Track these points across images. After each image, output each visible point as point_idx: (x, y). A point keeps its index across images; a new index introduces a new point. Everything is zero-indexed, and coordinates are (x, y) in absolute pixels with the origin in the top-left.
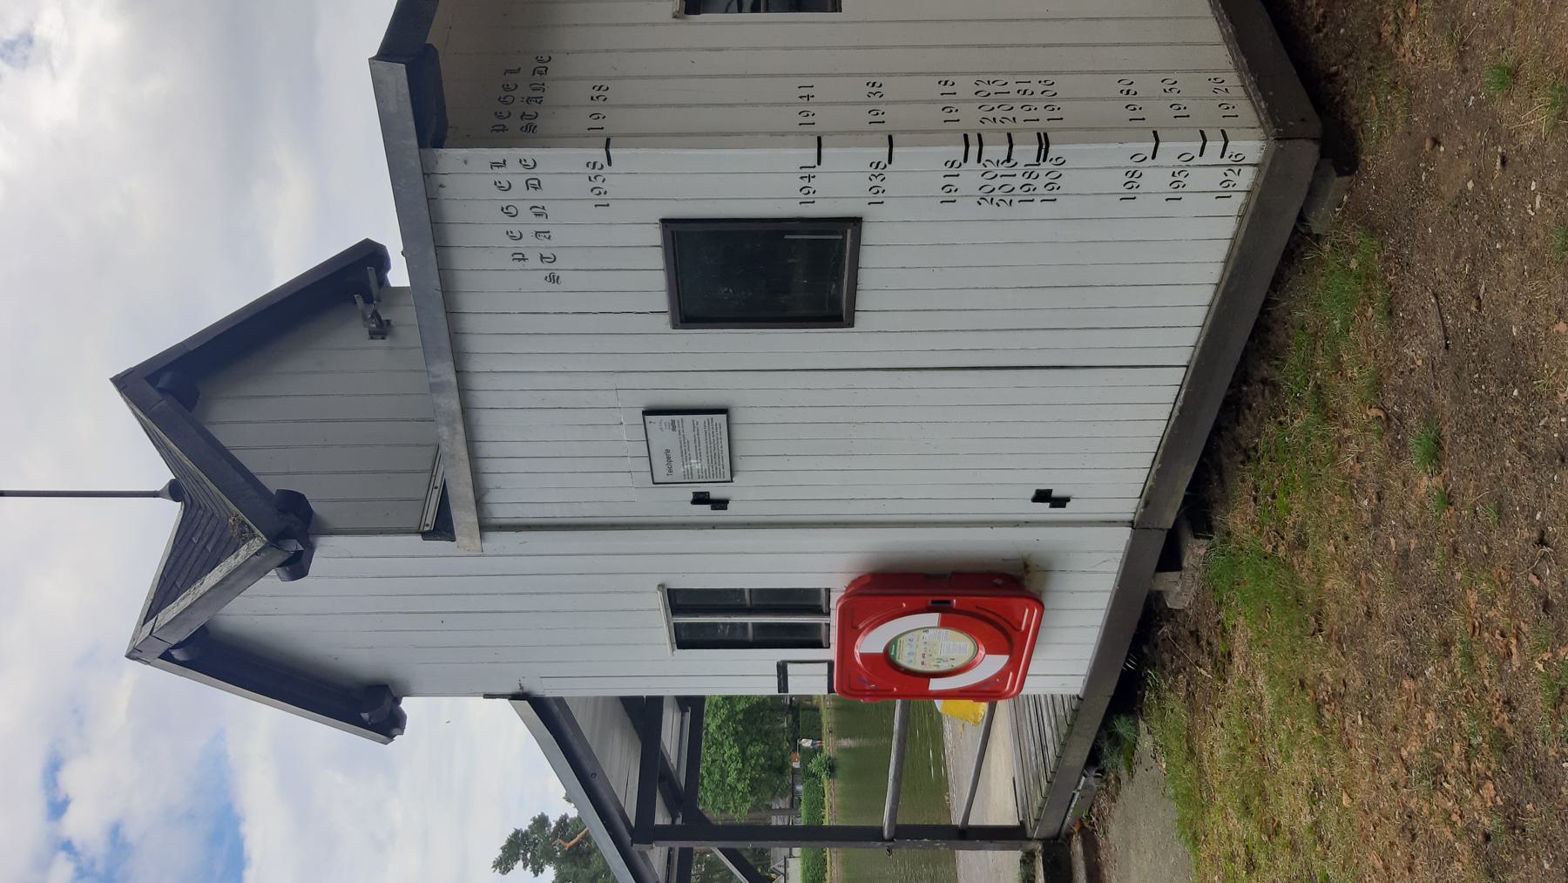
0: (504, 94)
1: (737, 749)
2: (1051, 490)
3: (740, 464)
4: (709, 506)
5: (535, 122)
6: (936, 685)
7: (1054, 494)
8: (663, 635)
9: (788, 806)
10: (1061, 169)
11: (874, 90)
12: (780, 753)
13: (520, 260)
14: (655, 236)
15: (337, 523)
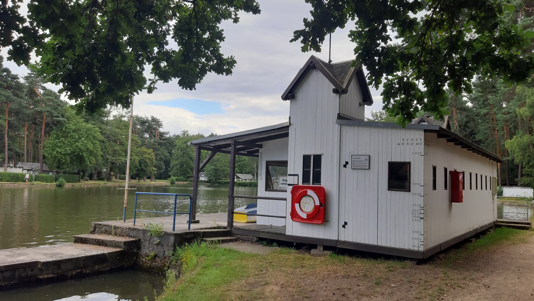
1: (69, 152)
3: (355, 171)
7: (346, 225)
8: (307, 153)
9: (44, 169)
12: (65, 167)
14: (407, 161)
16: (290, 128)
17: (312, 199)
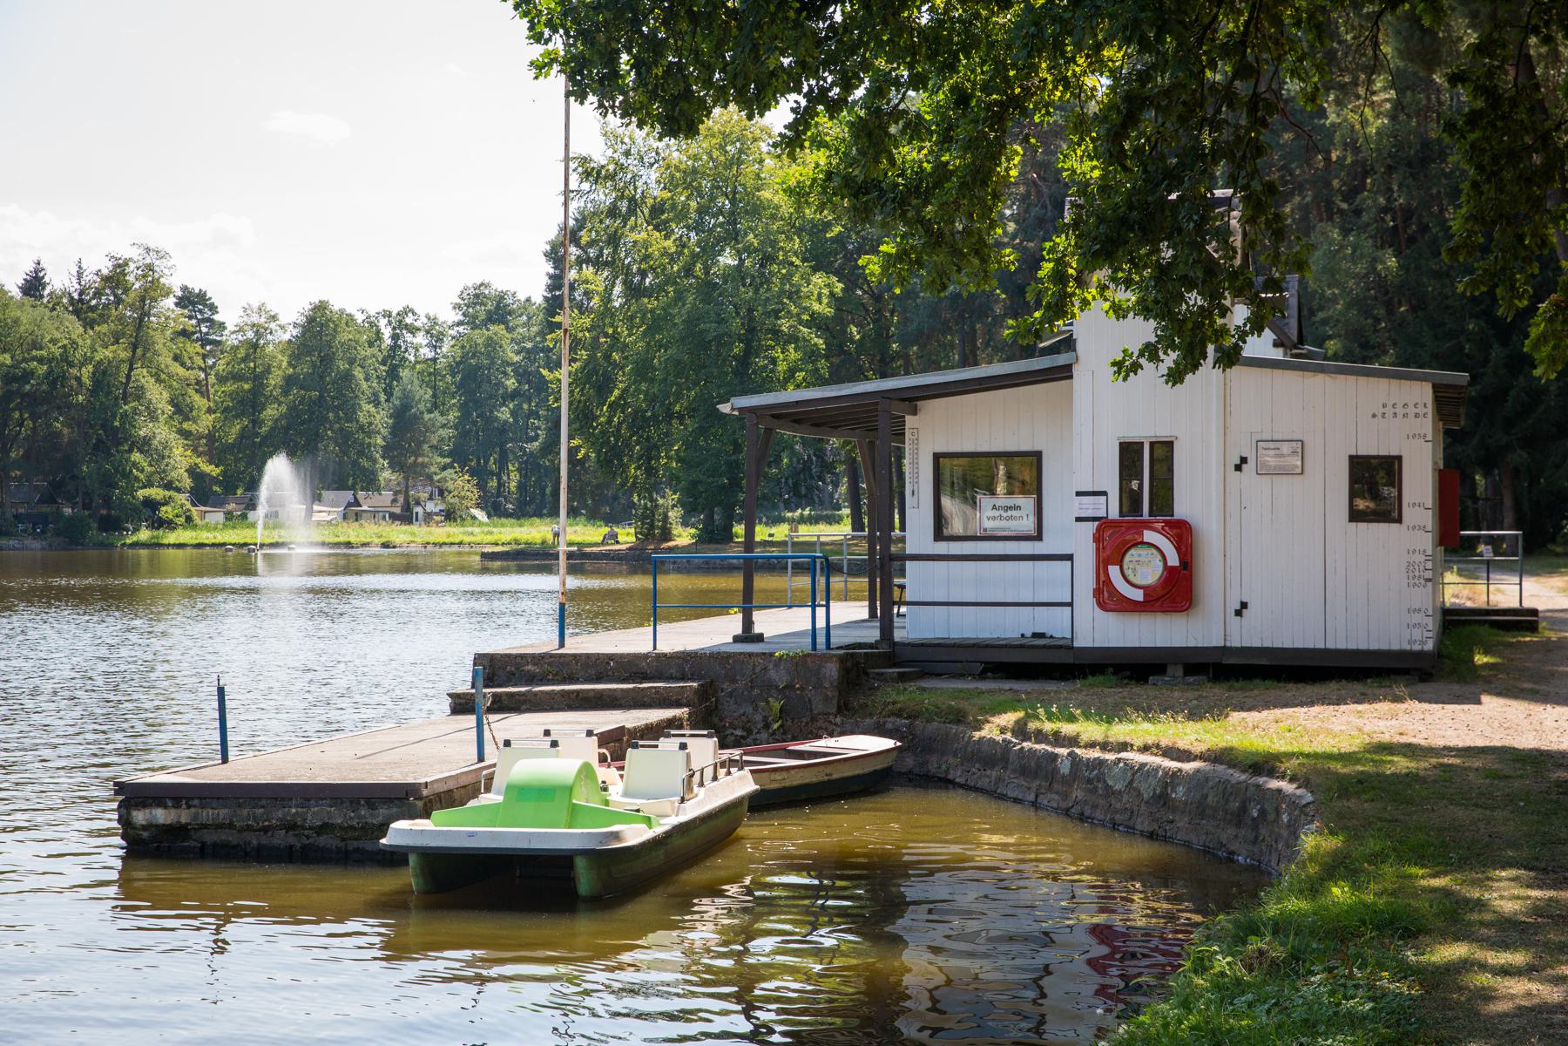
8: (1133, 434)
14: (1394, 453)
17: (1154, 551)
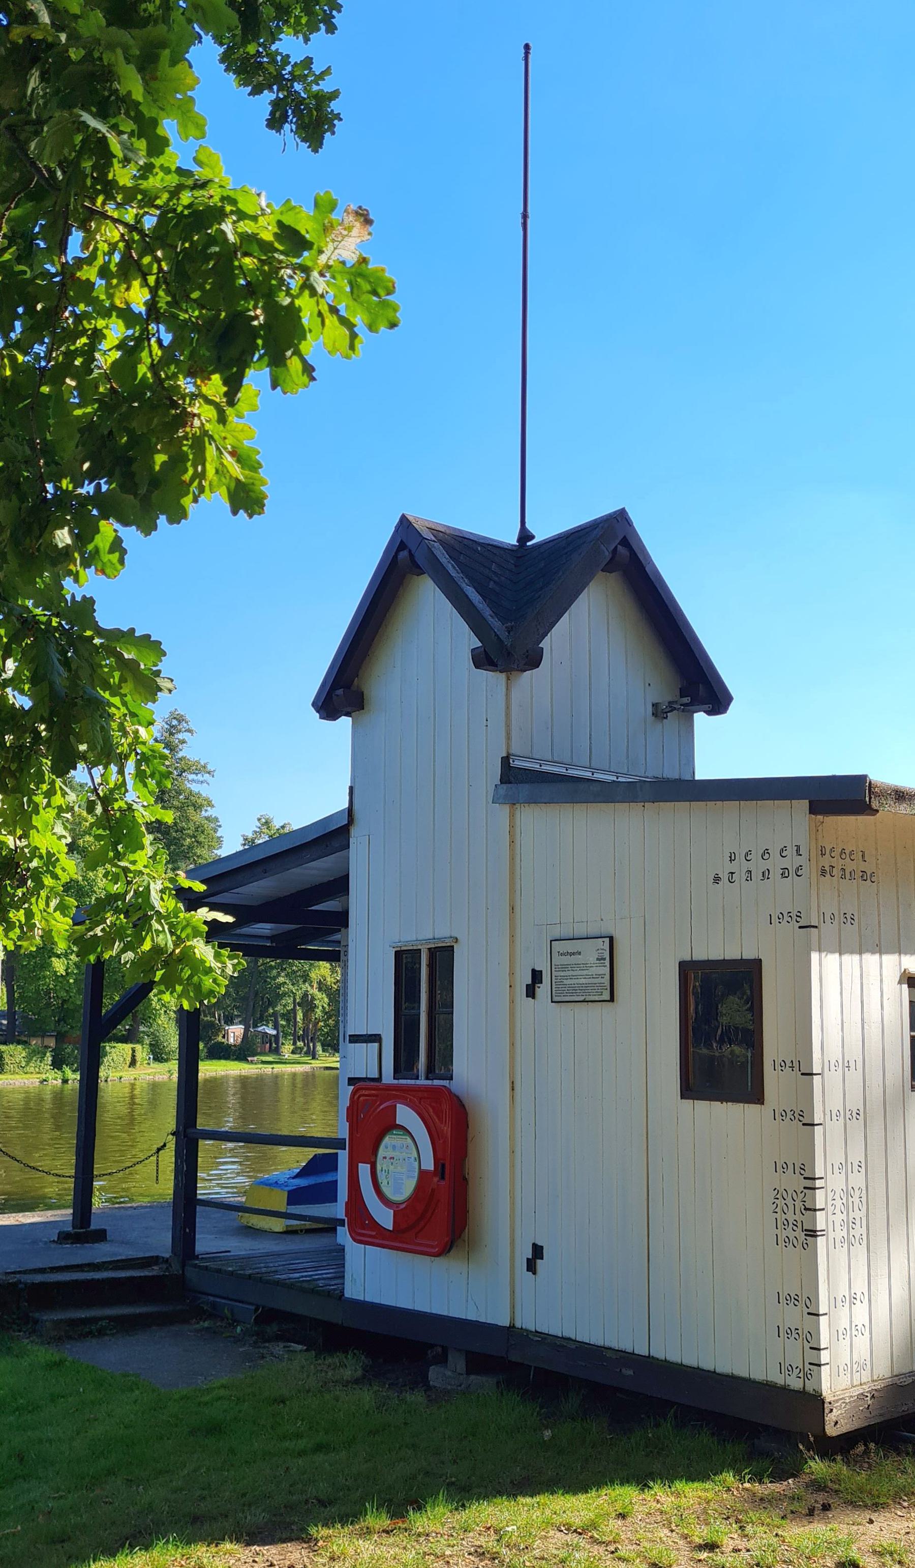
0: (847, 852)
2: (542, 1258)
4: (530, 982)
5: (828, 876)
6: (364, 1169)
7: (539, 1261)
10: (799, 1246)
11: (854, 1114)
13: (731, 857)
14: (749, 955)
15: (515, 694)
16: (354, 831)
17: (409, 1140)
